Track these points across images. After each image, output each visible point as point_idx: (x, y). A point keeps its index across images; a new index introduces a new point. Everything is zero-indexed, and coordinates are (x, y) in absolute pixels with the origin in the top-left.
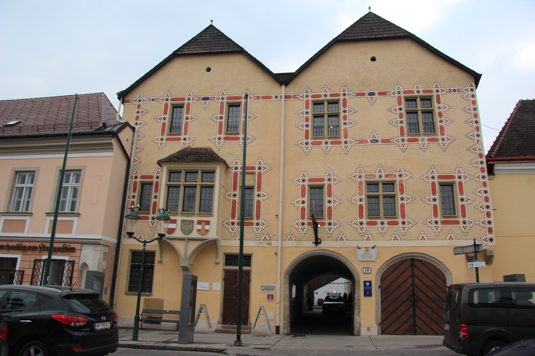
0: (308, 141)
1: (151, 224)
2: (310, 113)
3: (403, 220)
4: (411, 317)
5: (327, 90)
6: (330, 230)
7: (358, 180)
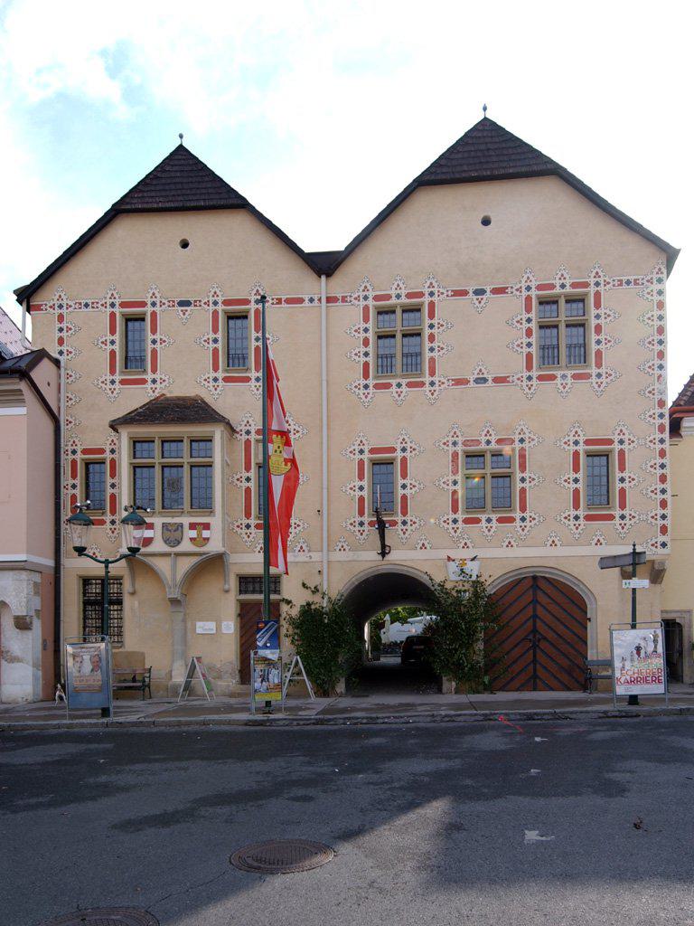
4: (529, 664)
7: (451, 449)
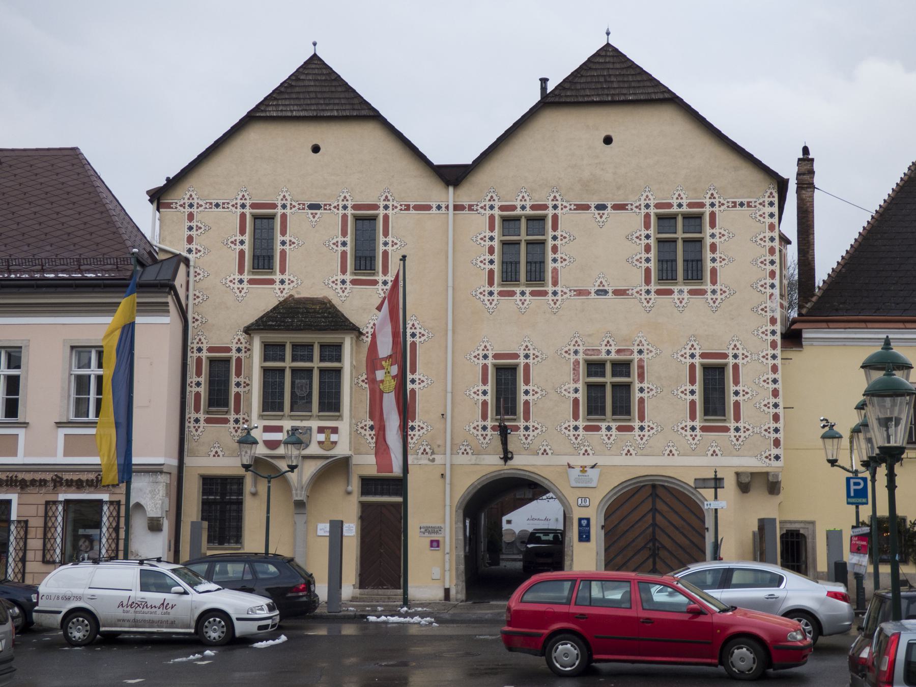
0: (492, 289)
1: (233, 431)
2: (496, 240)
3: (641, 424)
5: (526, 197)
6: (526, 439)
7: (573, 357)
